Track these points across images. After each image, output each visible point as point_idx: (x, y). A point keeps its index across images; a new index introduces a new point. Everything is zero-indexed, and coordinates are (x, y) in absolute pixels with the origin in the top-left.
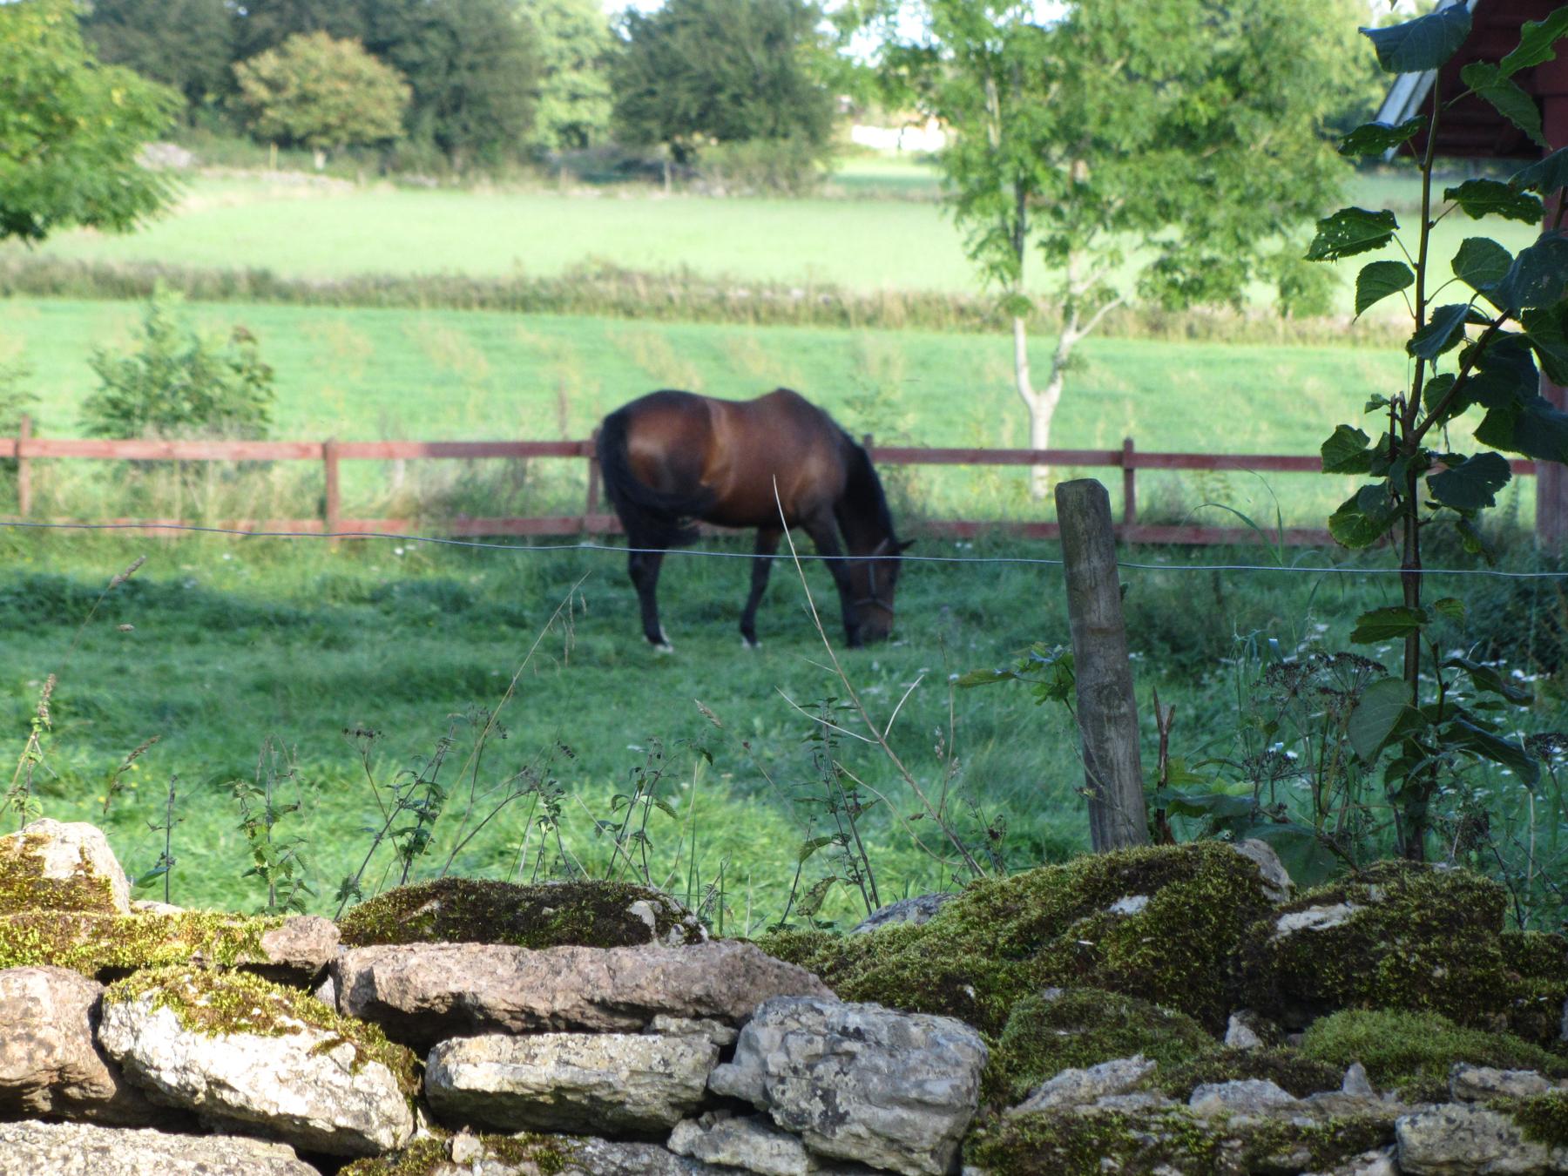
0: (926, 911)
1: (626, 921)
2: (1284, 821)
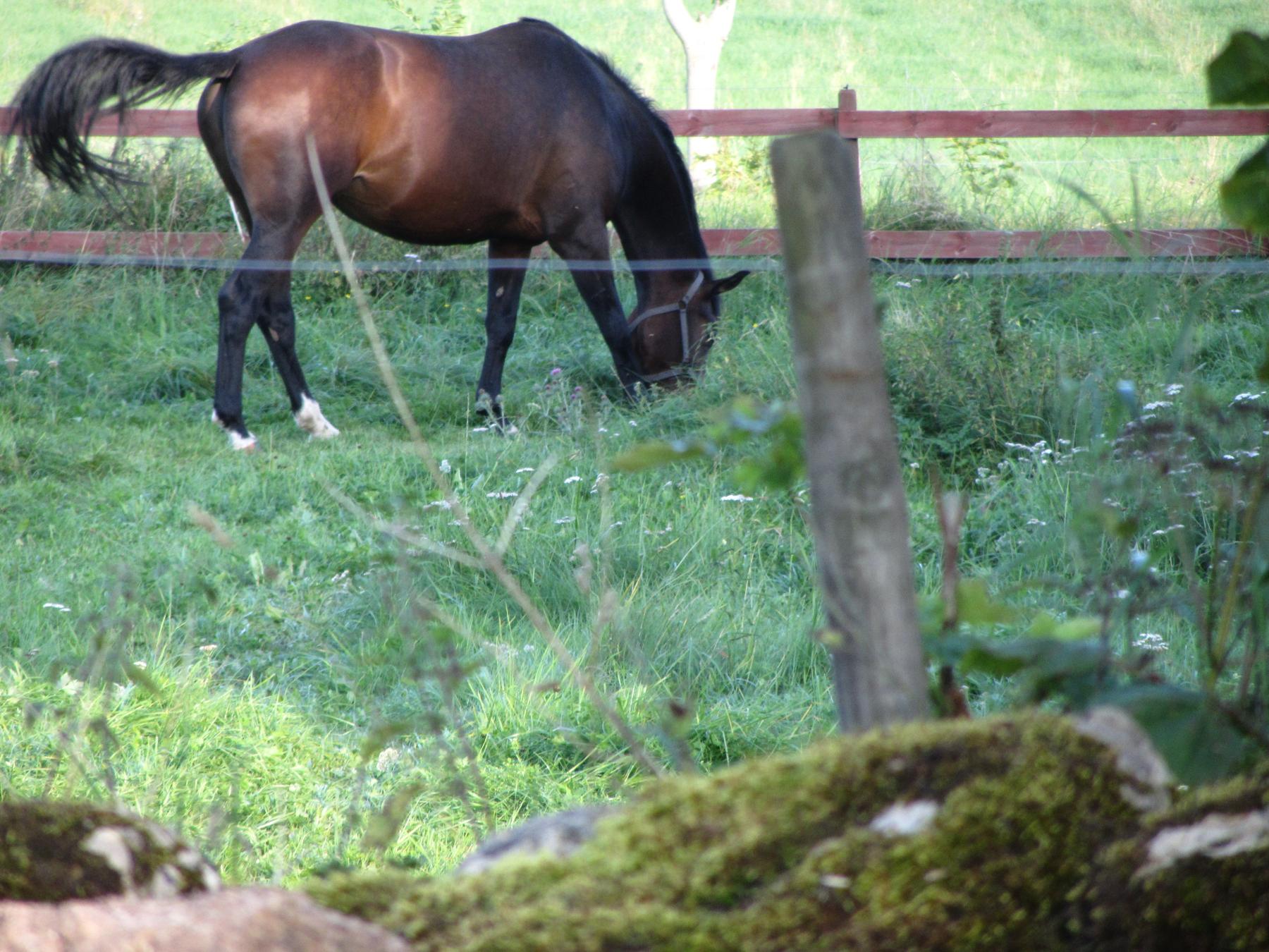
0: (573, 836)
1: (81, 863)
2: (1155, 679)
